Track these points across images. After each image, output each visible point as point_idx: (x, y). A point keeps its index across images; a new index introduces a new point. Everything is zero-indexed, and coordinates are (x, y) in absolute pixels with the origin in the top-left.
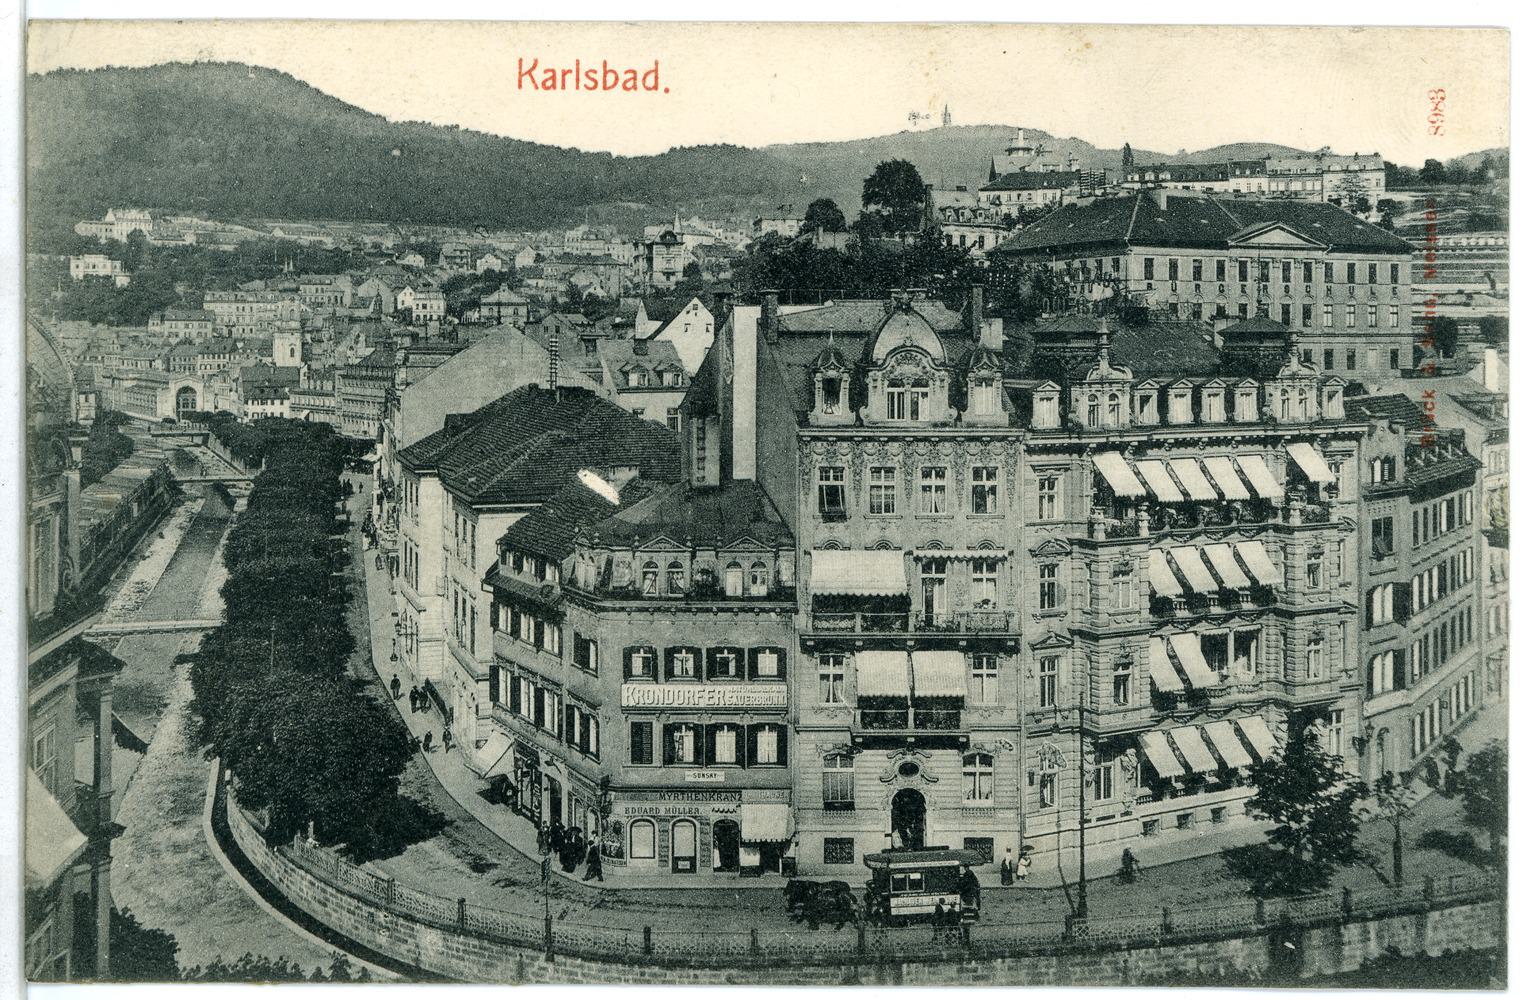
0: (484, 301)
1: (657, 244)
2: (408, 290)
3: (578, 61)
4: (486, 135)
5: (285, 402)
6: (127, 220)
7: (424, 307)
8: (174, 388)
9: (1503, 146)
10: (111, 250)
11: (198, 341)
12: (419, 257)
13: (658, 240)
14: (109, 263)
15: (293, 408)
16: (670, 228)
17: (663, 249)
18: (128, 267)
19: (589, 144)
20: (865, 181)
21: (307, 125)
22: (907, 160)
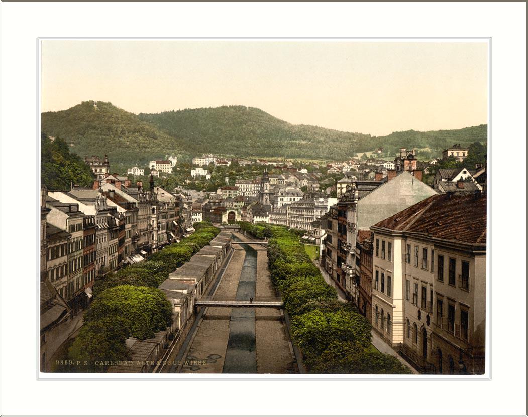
0: (339, 181)
1: (406, 159)
2: (306, 180)
3: (414, 278)
4: (126, 112)
5: (267, 217)
6: (209, 157)
7: (312, 186)
8: (228, 212)
9: (486, 124)
10: (204, 167)
11: (233, 197)
12: (306, 170)
13: (406, 158)
14: (204, 170)
15: (271, 219)
16: (411, 153)
17: (408, 162)
18: (210, 172)
19: (193, 374)
20: (370, 135)
21: (433, 137)
22: (395, 131)
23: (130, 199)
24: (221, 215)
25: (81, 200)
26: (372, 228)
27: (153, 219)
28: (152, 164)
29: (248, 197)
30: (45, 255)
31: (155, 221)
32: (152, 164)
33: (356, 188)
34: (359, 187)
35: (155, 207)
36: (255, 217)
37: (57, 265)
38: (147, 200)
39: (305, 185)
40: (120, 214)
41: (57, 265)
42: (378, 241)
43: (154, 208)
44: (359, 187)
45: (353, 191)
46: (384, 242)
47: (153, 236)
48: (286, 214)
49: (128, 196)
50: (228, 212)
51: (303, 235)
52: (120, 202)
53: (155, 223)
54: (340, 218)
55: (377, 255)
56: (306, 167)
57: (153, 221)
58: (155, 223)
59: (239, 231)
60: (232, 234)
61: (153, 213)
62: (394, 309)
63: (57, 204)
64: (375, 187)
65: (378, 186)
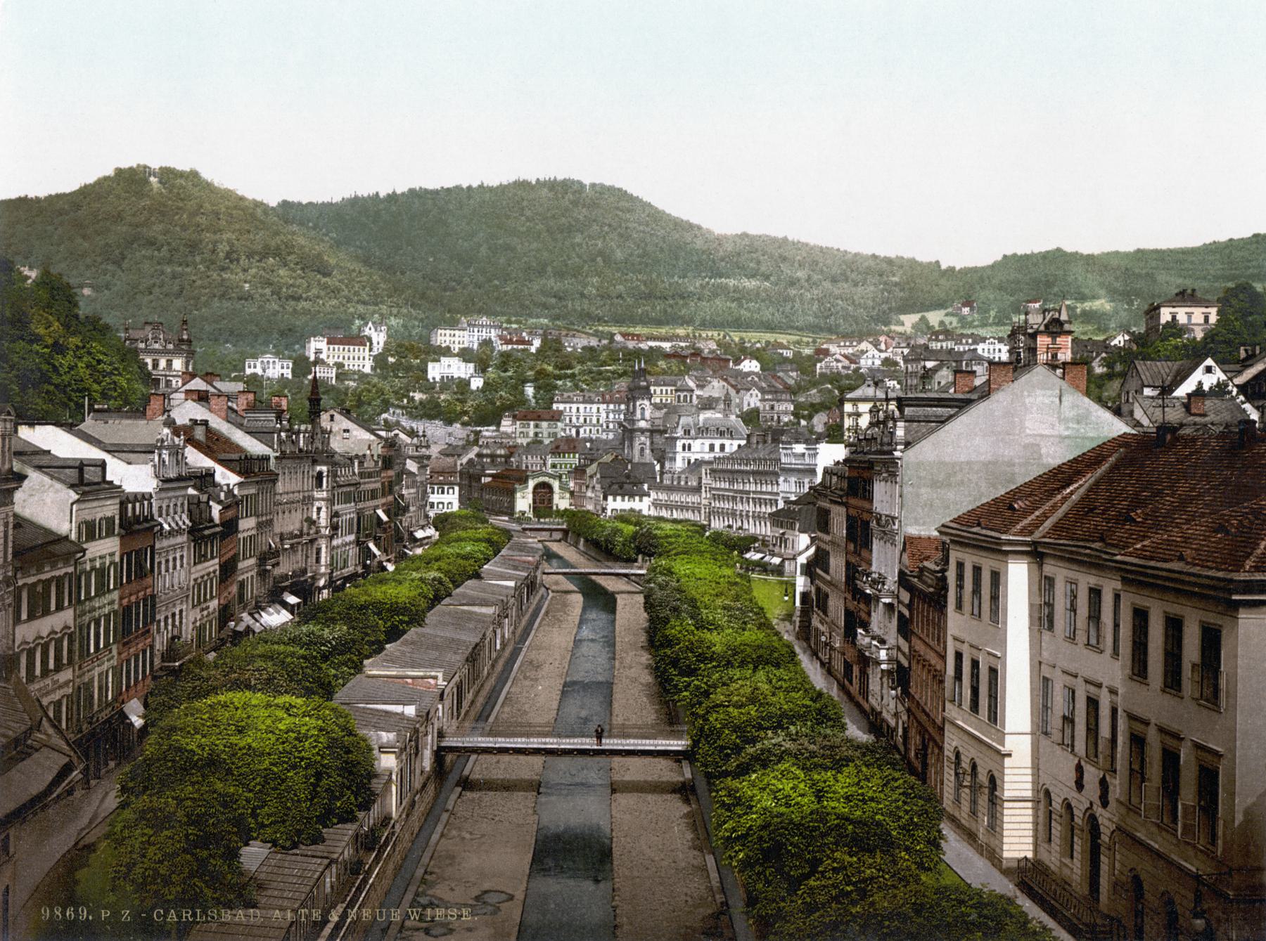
8: (531, 484)
11: (547, 442)
23: (254, 447)
24: (511, 494)
25: (114, 450)
26: (944, 530)
27: (317, 504)
28: (317, 346)
29: (591, 440)
30: (9, 605)
31: (324, 509)
32: (317, 346)
33: (897, 413)
34: (907, 411)
35: (324, 468)
36: (610, 498)
37: (44, 634)
38: (301, 450)
39: (752, 405)
40: (225, 488)
41: (44, 634)
42: (960, 566)
43: (320, 473)
44: (907, 411)
45: (890, 424)
46: (977, 570)
47: (319, 551)
48: (697, 490)
49: (248, 437)
50: (531, 484)
51: (748, 550)
52: (223, 456)
53: (323, 514)
54: (853, 501)
55: (959, 606)
56: (755, 355)
57: (319, 509)
58: (323, 514)
59: (565, 538)
60: (545, 547)
61: (320, 485)
62: (1007, 760)
63: (45, 461)
64: (952, 411)
65: (961, 408)
